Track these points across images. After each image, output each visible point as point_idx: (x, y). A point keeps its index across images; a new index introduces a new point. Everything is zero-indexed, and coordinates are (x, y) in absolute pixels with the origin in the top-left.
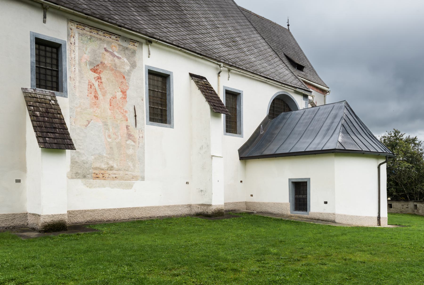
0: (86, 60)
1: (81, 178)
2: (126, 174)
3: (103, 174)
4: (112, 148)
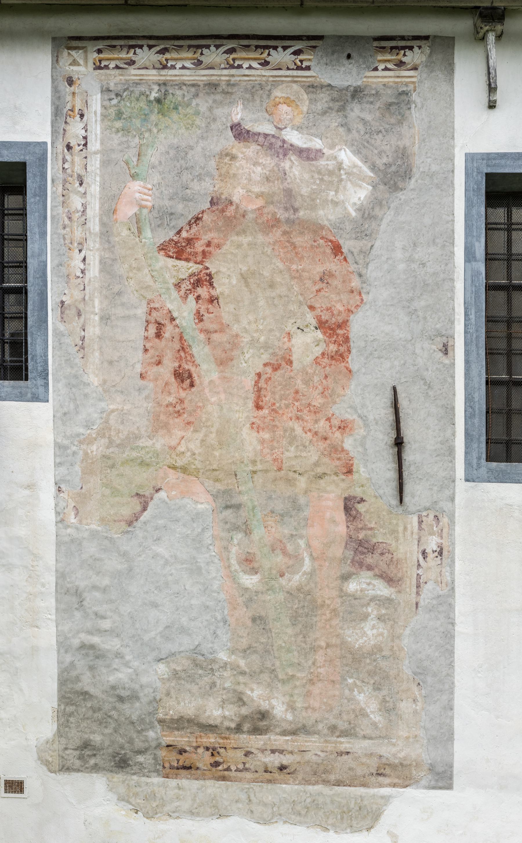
0: (135, 210)
1: (104, 769)
2: (341, 754)
3: (213, 751)
4: (261, 618)
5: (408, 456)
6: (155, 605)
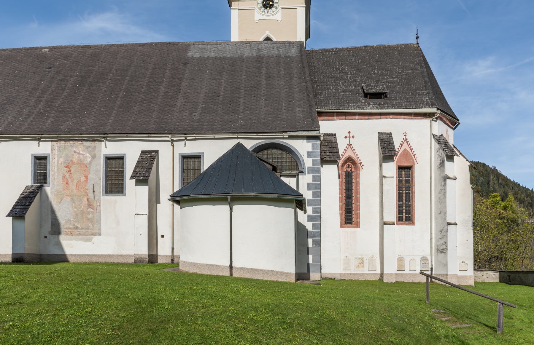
3: (71, 232)
5: (95, 193)
6: (63, 213)
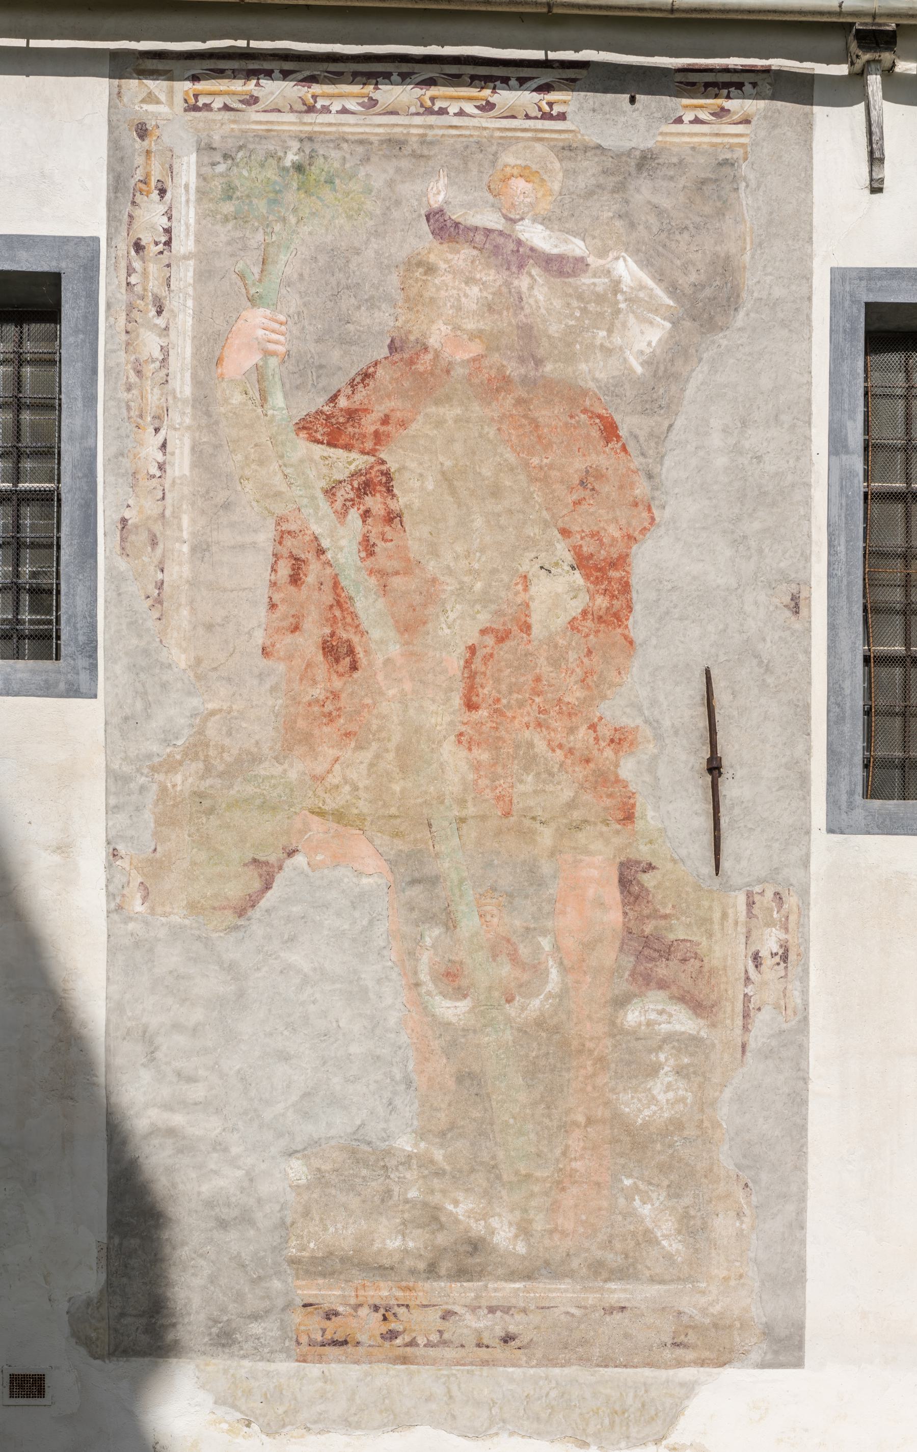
0: (257, 358)
3: (386, 1313)
4: (471, 1075)
